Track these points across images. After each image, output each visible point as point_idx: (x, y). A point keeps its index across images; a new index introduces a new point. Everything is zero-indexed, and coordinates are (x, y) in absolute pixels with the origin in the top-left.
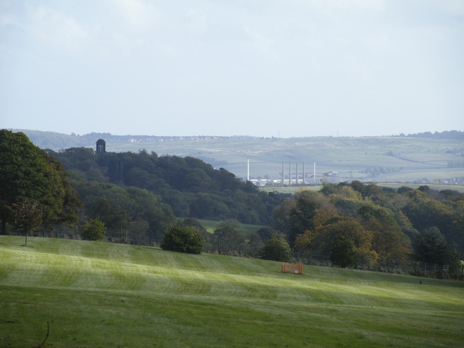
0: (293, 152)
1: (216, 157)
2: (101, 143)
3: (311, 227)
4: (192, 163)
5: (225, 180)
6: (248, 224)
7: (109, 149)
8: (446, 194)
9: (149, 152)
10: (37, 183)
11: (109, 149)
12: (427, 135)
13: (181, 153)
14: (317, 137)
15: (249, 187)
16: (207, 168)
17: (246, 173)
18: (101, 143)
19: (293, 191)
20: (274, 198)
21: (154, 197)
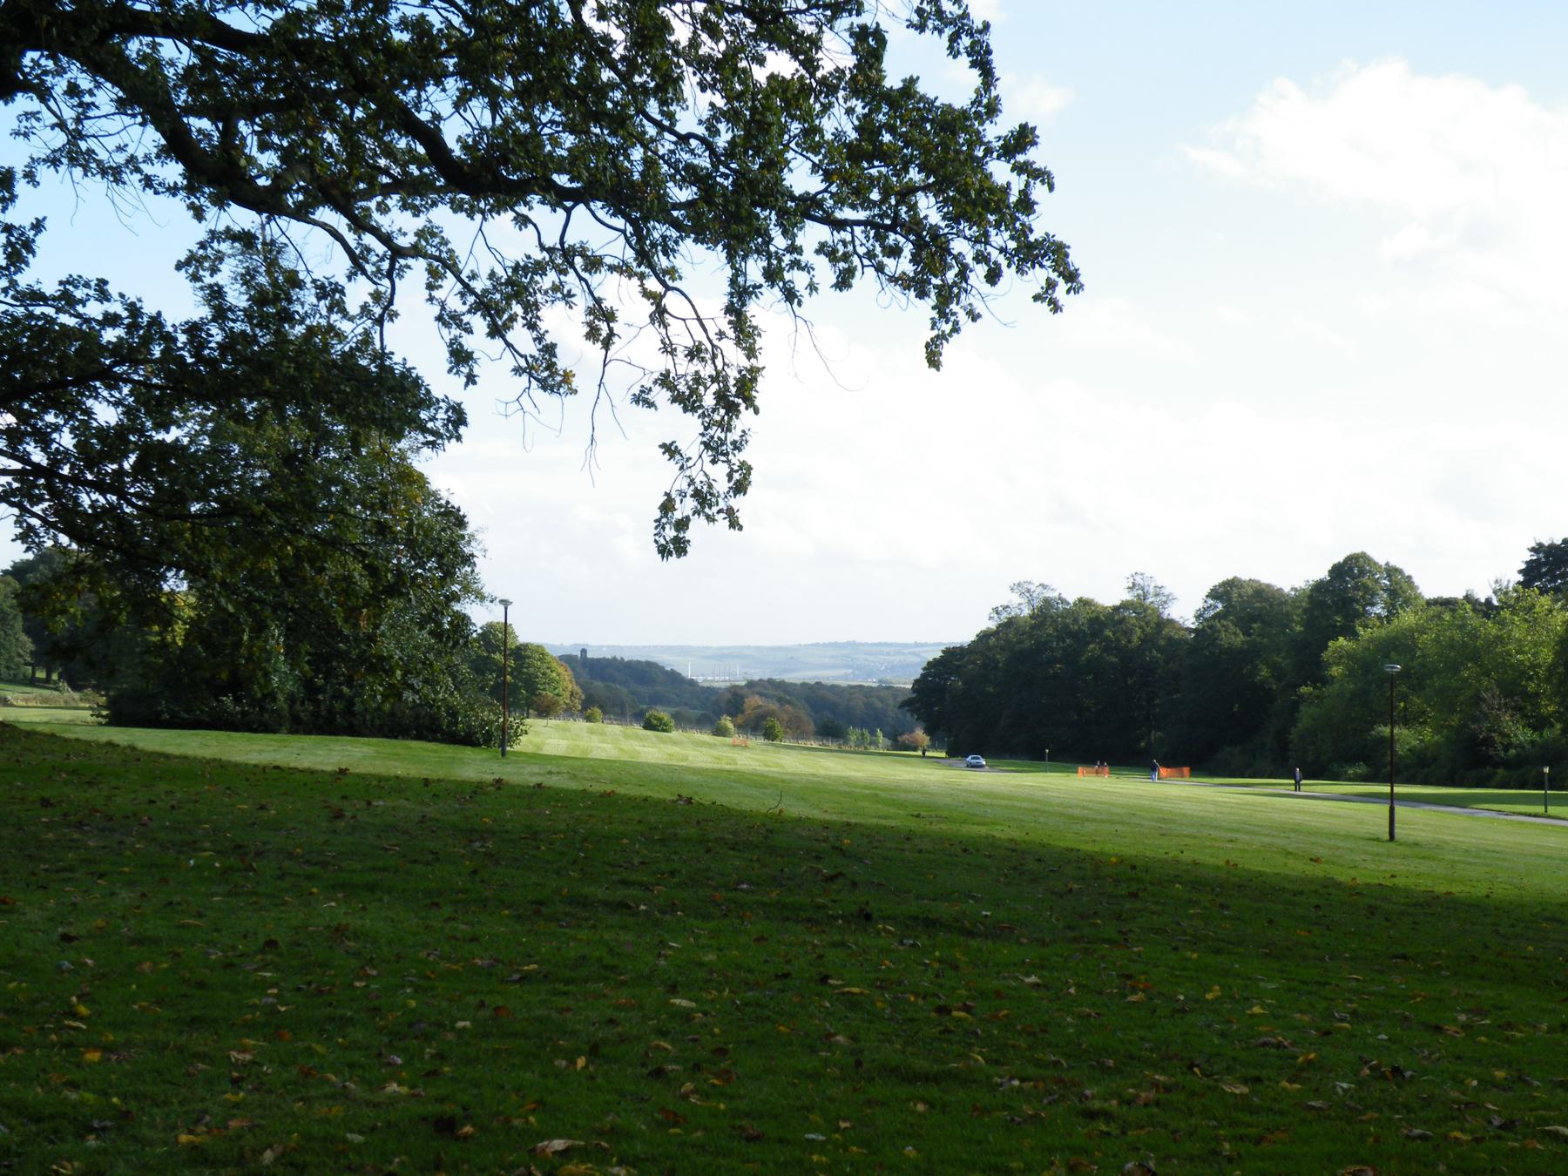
0: (723, 655)
1: (669, 661)
2: (584, 651)
3: (742, 712)
4: (650, 665)
5: (674, 678)
6: (353, 730)
7: (589, 655)
8: (833, 687)
9: (1528, 556)
10: (552, 680)
11: (589, 655)
12: (817, 645)
13: (641, 657)
14: (1269, 586)
15: (692, 683)
16: (661, 669)
17: (688, 673)
18: (584, 651)
19: (723, 685)
20: (710, 691)
21: (624, 690)
